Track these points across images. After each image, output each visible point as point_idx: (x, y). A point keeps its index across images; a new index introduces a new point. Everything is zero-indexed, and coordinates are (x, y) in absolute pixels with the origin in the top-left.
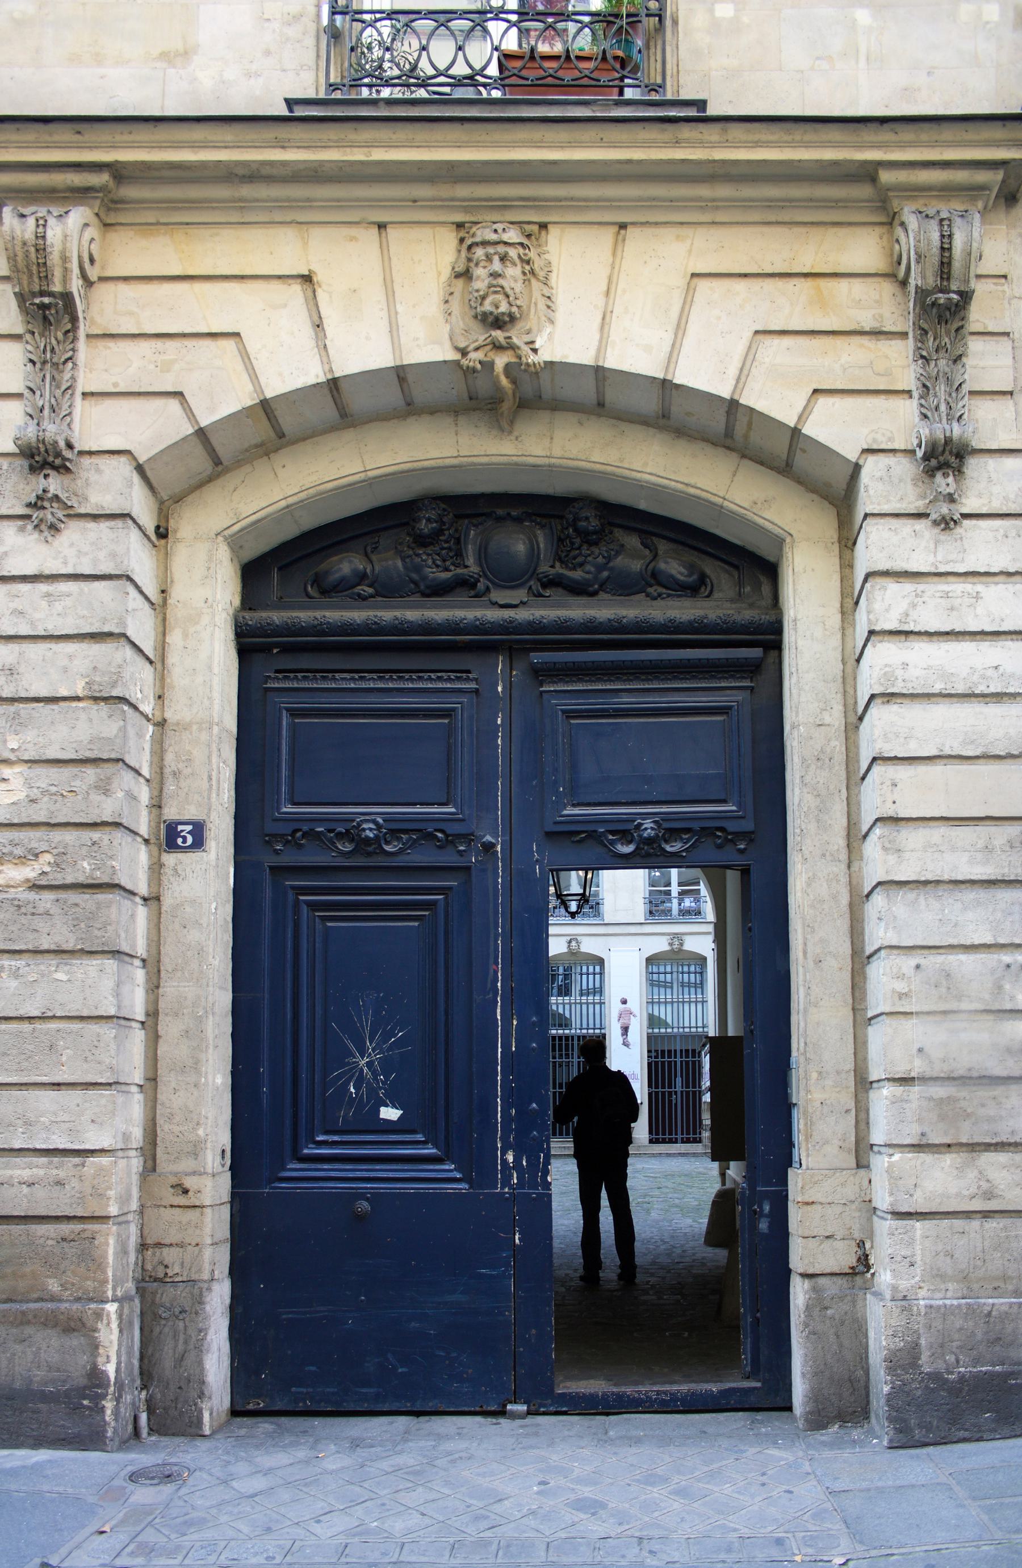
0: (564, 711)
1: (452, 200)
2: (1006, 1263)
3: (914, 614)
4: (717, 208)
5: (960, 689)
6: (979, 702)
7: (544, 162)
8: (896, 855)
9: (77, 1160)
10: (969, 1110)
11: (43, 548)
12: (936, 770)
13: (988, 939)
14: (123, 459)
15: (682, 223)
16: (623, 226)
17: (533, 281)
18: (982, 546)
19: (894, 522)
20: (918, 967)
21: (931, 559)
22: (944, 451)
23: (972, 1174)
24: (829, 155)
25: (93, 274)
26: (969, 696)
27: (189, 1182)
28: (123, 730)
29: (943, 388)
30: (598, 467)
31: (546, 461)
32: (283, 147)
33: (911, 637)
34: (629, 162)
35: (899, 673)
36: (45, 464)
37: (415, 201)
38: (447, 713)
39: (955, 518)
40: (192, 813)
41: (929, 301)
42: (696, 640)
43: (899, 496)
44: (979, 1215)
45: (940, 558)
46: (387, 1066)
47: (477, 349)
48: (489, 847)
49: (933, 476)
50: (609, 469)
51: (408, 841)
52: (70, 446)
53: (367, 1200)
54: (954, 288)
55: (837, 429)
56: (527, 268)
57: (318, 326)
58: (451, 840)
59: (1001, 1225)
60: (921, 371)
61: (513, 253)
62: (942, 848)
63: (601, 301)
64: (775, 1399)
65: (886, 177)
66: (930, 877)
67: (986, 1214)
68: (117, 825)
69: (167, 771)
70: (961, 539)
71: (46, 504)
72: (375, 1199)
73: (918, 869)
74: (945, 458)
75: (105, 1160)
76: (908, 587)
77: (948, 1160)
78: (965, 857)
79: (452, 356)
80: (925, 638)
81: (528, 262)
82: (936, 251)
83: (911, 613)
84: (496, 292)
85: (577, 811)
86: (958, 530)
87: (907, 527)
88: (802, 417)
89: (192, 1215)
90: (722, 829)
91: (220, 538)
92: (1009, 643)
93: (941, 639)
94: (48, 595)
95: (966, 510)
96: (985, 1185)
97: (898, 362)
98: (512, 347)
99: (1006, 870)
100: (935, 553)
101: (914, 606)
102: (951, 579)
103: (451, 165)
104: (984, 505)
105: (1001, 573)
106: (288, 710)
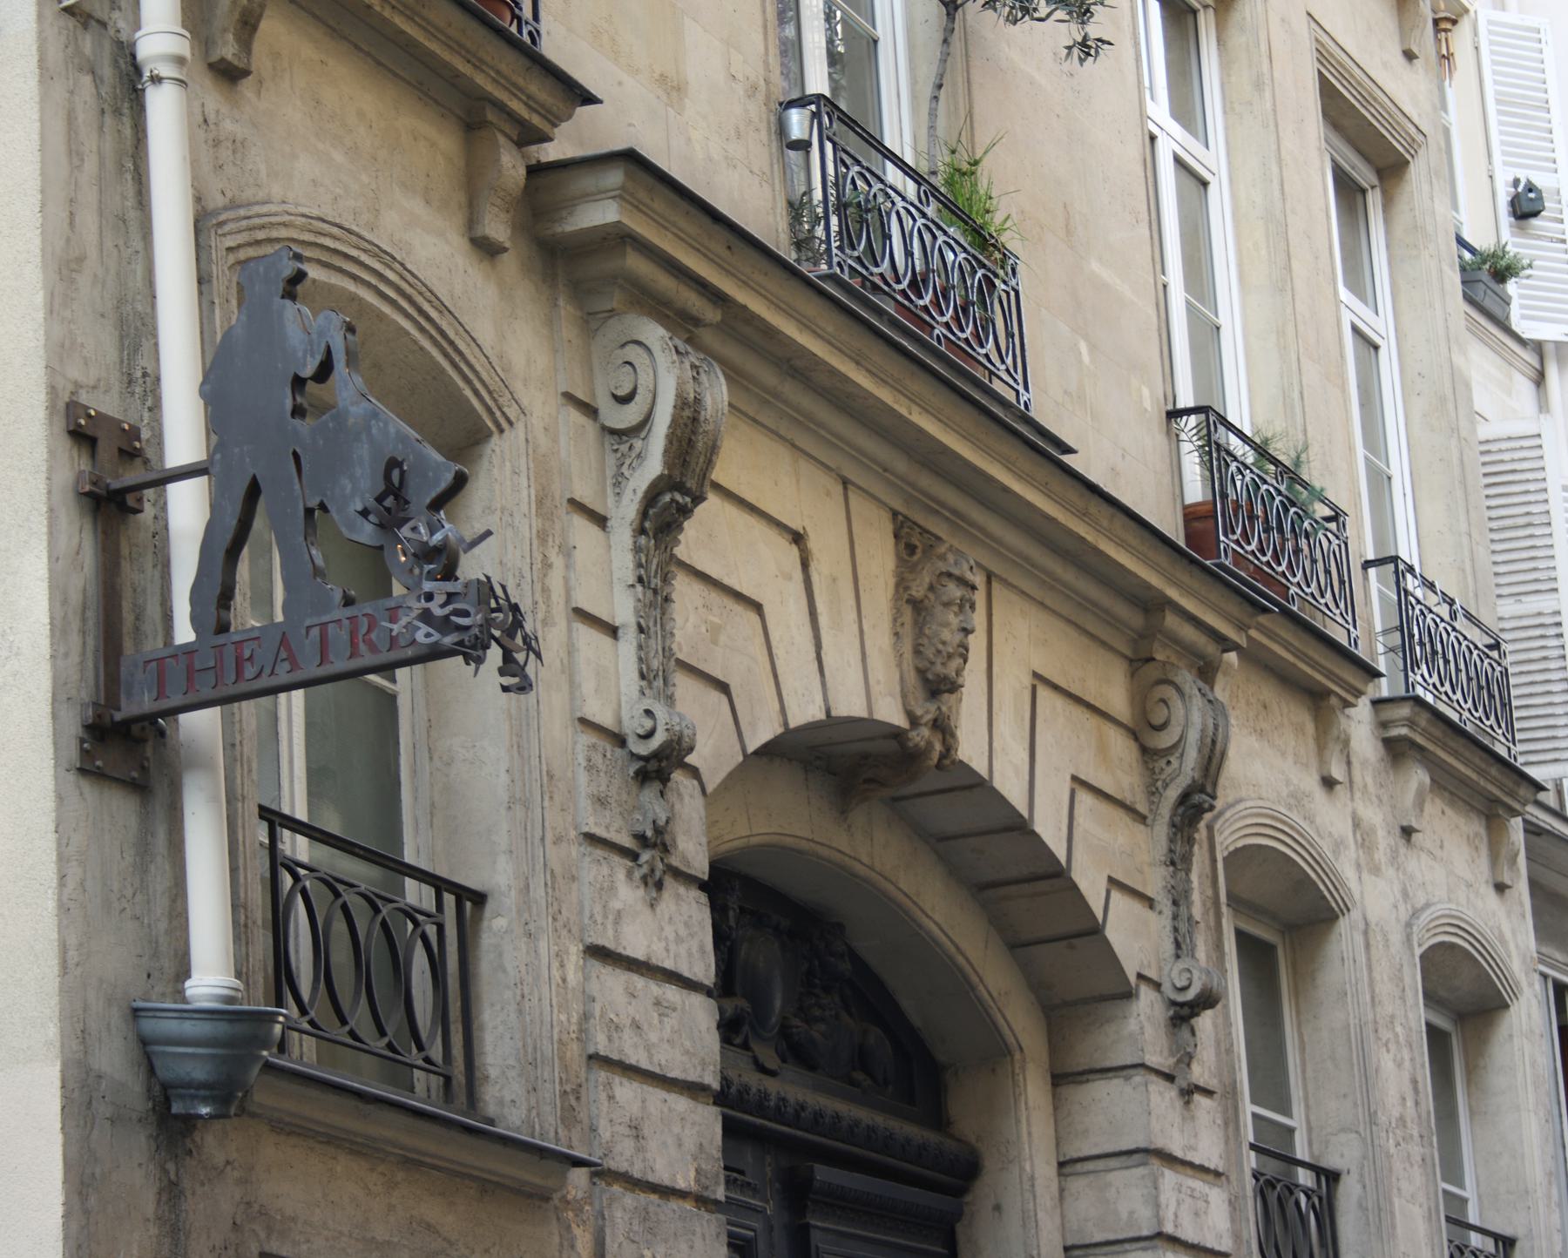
4: (1052, 588)
30: (901, 897)
32: (858, 363)
37: (885, 470)
65: (1171, 621)
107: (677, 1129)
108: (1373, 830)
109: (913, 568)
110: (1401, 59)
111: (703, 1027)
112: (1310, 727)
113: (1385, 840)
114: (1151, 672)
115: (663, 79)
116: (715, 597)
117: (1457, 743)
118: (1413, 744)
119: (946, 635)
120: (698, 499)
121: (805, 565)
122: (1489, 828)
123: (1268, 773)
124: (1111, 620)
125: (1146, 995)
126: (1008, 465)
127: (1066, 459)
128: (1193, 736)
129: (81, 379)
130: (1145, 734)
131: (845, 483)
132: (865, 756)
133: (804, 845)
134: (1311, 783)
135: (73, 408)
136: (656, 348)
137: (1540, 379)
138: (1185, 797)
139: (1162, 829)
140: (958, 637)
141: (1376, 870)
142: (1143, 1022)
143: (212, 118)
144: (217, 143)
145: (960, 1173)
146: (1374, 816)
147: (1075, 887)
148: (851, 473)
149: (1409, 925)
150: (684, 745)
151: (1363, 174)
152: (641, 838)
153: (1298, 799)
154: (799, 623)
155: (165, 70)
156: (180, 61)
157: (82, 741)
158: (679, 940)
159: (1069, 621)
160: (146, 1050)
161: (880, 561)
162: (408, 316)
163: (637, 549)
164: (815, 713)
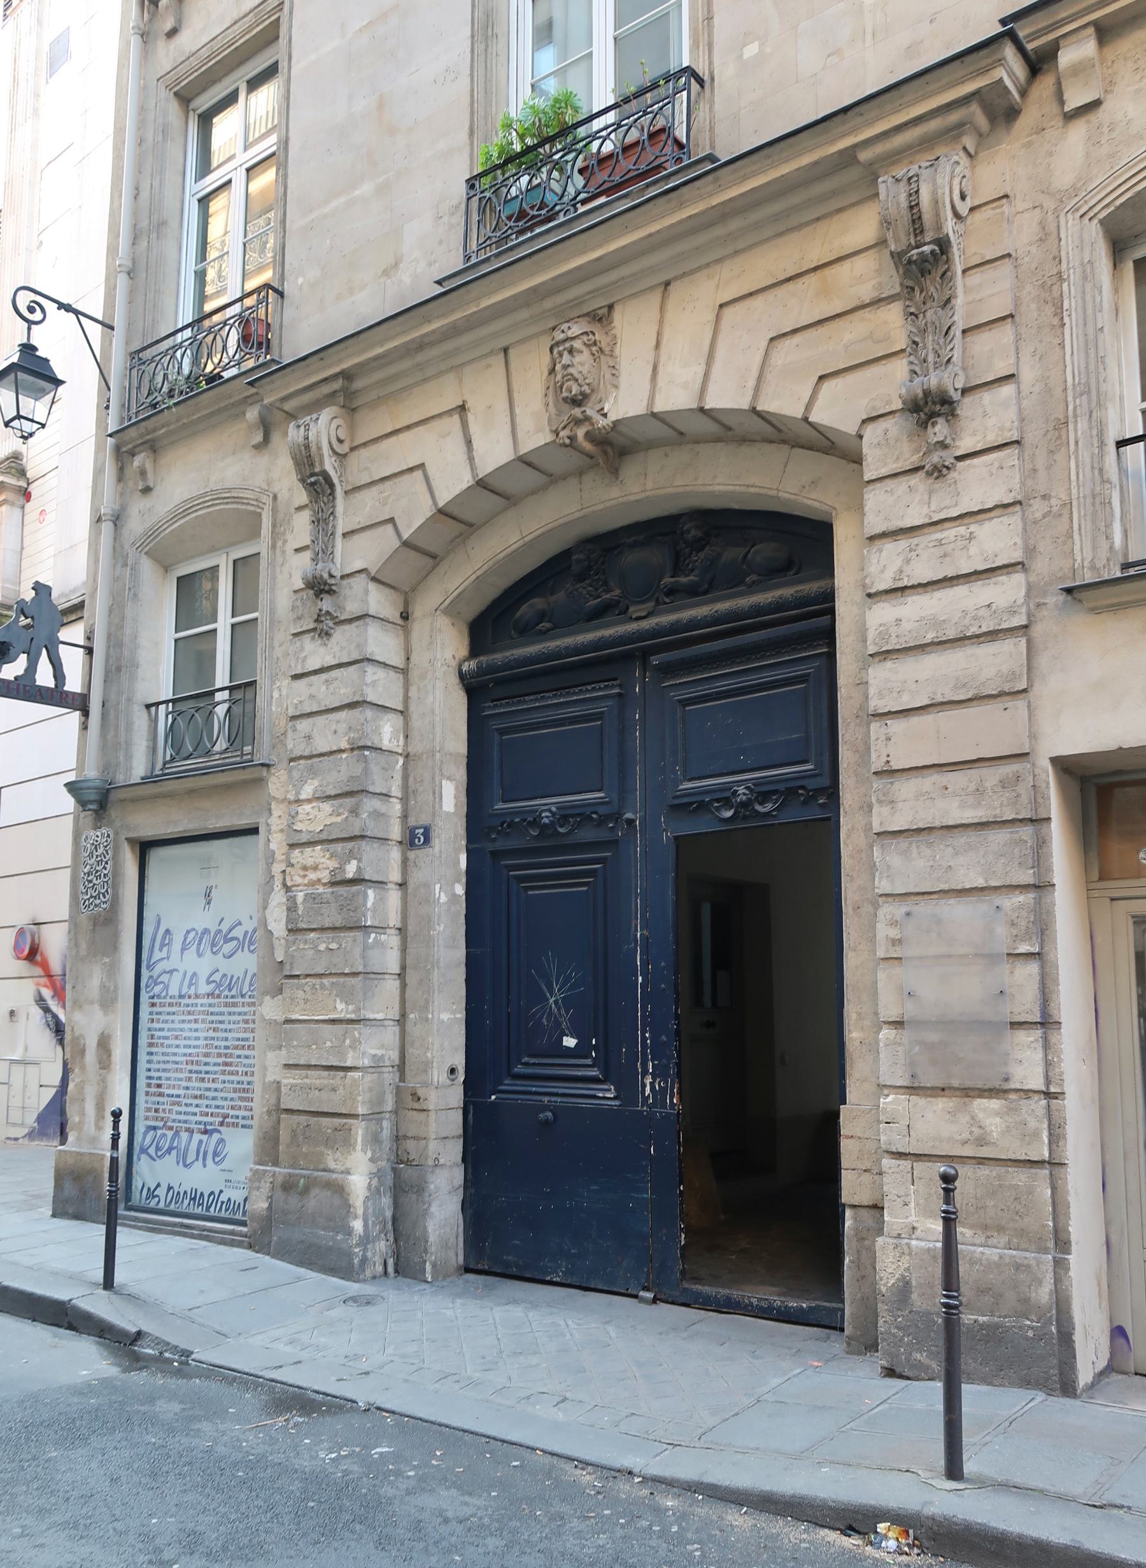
0: (679, 701)
1: (544, 312)
2: (999, 1212)
3: (907, 570)
5: (951, 634)
6: (973, 644)
7: (553, 279)
8: (890, 806)
9: (342, 1074)
10: (961, 1055)
11: (322, 650)
12: (928, 719)
13: (980, 882)
14: (363, 576)
15: (818, 219)
16: (667, 284)
17: (602, 357)
18: (979, 485)
19: (890, 484)
20: (908, 914)
21: (925, 510)
22: (926, 403)
23: (964, 1119)
24: (806, 160)
25: (963, 208)
26: (961, 640)
27: (421, 1093)
28: (366, 770)
29: (930, 338)
31: (643, 495)
33: (907, 592)
34: (650, 235)
35: (893, 631)
36: (322, 591)
38: (599, 716)
39: (947, 464)
40: (424, 820)
41: (904, 260)
42: (822, 609)
43: (895, 457)
44: (973, 1161)
45: (933, 508)
46: (567, 1002)
47: (564, 428)
48: (631, 822)
49: (926, 427)
50: (688, 488)
51: (574, 823)
52: (331, 576)
53: (551, 1111)
54: (928, 239)
55: (836, 411)
56: (594, 349)
57: (469, 442)
58: (602, 821)
59: (994, 1174)
60: (910, 328)
61: (577, 344)
62: (932, 795)
63: (652, 353)
65: (864, 156)
66: (921, 825)
67: (981, 1161)
68: (363, 837)
69: (410, 790)
70: (955, 482)
71: (323, 619)
73: (910, 818)
74: (930, 408)
75: (357, 1075)
76: (903, 544)
77: (941, 1104)
78: (955, 803)
80: (920, 590)
81: (595, 343)
82: (905, 212)
83: (905, 569)
84: (568, 380)
85: (690, 785)
86: (953, 475)
87: (902, 484)
88: (809, 407)
89: (423, 1115)
90: (802, 787)
91: (439, 612)
92: (1003, 578)
93: (935, 587)
95: (959, 453)
96: (977, 1131)
97: (892, 323)
98: (587, 419)
99: (998, 811)
100: (929, 504)
101: (908, 561)
102: (947, 525)
103: (534, 290)
104: (978, 442)
105: (996, 507)
106: (496, 730)
107: (334, 727)
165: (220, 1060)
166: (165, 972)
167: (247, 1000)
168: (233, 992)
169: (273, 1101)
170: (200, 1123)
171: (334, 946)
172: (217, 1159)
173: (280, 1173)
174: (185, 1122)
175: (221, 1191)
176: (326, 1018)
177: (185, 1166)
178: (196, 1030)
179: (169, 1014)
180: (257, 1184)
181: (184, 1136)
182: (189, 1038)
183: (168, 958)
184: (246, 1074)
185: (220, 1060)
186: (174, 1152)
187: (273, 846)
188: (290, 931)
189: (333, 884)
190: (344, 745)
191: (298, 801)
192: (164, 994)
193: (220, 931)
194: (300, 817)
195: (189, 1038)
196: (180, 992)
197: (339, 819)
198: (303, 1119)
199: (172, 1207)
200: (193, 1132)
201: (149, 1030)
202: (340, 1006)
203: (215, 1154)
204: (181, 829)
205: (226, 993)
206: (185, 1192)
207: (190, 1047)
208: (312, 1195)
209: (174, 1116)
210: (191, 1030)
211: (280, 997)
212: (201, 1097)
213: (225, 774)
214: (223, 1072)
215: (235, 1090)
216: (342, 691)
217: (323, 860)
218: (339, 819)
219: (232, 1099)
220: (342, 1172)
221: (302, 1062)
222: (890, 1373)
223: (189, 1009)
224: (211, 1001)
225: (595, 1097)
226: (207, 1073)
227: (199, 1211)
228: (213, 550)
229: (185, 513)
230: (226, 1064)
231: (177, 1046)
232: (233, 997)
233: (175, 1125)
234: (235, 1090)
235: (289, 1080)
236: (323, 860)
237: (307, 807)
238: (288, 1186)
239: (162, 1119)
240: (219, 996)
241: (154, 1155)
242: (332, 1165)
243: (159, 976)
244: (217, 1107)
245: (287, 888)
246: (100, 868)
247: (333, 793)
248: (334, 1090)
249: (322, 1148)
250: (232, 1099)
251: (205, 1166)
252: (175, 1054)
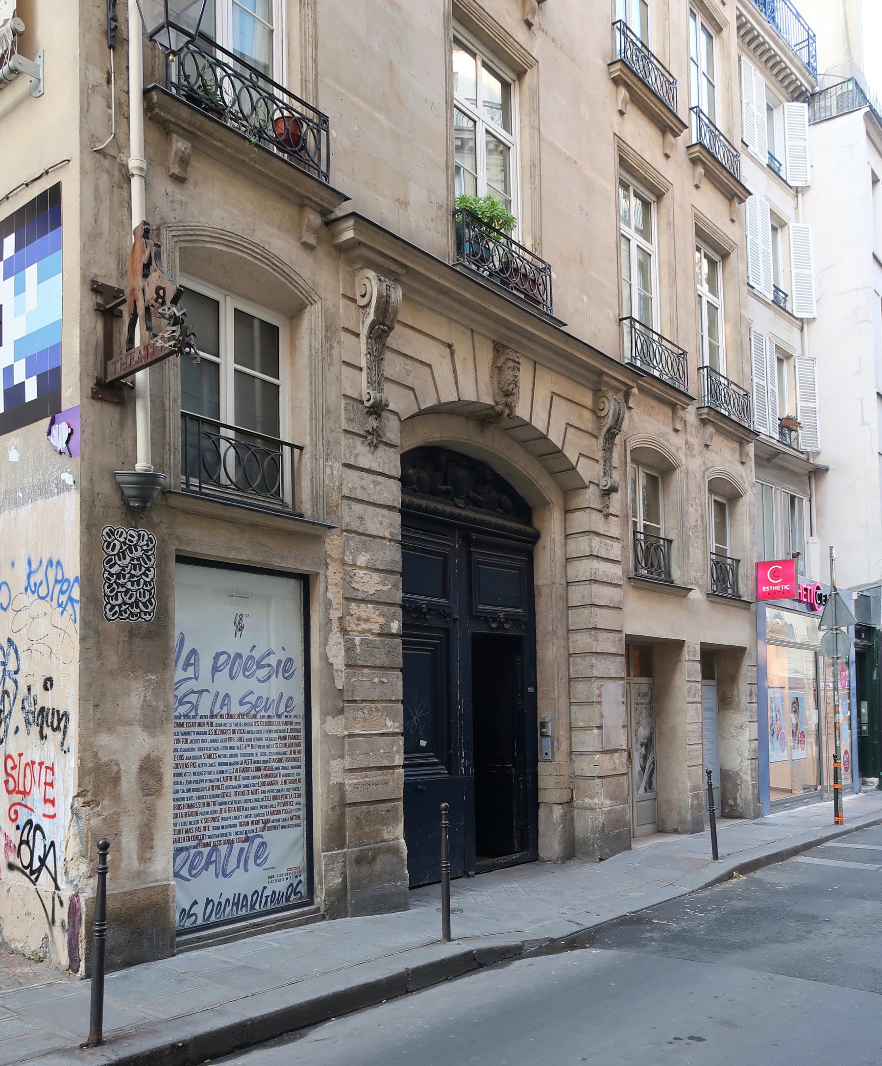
7: (517, 325)
11: (370, 455)
64: (535, 858)
65: (605, 378)
72: (425, 783)
79: (493, 404)
90: (520, 620)
94: (374, 481)
107: (380, 519)
108: (693, 445)
109: (498, 358)
110: (730, 222)
111: (394, 490)
112: (670, 414)
113: (697, 448)
114: (601, 393)
115: (398, 200)
116: (409, 362)
117: (727, 421)
118: (710, 421)
119: (508, 377)
120: (391, 329)
121: (452, 354)
122: (740, 446)
123: (645, 424)
124: (587, 379)
125: (592, 488)
126: (534, 327)
127: (562, 328)
128: (611, 412)
129: (98, 273)
130: (596, 412)
131: (472, 331)
132: (487, 415)
133: (465, 441)
134: (669, 430)
135: (94, 282)
136: (372, 279)
137: (802, 329)
138: (609, 430)
139: (601, 440)
140: (513, 378)
141: (693, 456)
142: (590, 497)
143: (170, 193)
144: (172, 202)
145: (536, 537)
146: (694, 441)
147: (565, 455)
148: (474, 327)
149: (704, 472)
150: (383, 402)
151: (716, 257)
152: (368, 432)
153: (663, 435)
154: (447, 370)
155: (135, 172)
156: (141, 169)
157: (92, 389)
158: (384, 463)
159: (569, 378)
160: (119, 487)
161: (486, 355)
162: (267, 265)
163: (367, 343)
164: (453, 398)
165: (259, 773)
166: (193, 692)
167: (283, 719)
168: (270, 713)
169: (337, 799)
170: (241, 833)
171: (385, 680)
172: (259, 861)
173: (352, 852)
174: (225, 835)
175: (265, 888)
176: (381, 732)
177: (225, 875)
178: (232, 748)
179: (198, 733)
180: (331, 866)
181: (223, 849)
182: (225, 756)
183: (196, 678)
184: (286, 782)
185: (259, 773)
186: (212, 867)
187: (329, 595)
188: (347, 666)
189: (379, 635)
190: (388, 535)
191: (354, 565)
192: (193, 713)
193: (252, 657)
194: (355, 578)
195: (225, 756)
196: (212, 712)
197: (385, 588)
198: (365, 808)
199: (213, 919)
200: (233, 842)
201: (176, 750)
202: (389, 723)
203: (257, 857)
204: (244, 558)
205: (263, 713)
206: (228, 900)
207: (226, 764)
208: (378, 860)
209: (211, 832)
210: (226, 748)
211: (340, 717)
212: (239, 809)
213: (279, 519)
214: (263, 784)
215: (274, 798)
216: (386, 495)
217: (373, 616)
218: (385, 588)
219: (271, 806)
220: (393, 840)
221: (363, 766)
222: (601, 860)
223: (222, 728)
224: (246, 720)
225: (440, 774)
226: (246, 786)
227: (243, 912)
228: (227, 288)
229: (229, 244)
230: (266, 776)
231: (211, 765)
232: (269, 717)
233: (212, 840)
234: (274, 798)
235: (349, 781)
236: (373, 616)
237: (362, 573)
238: (359, 860)
239: (196, 838)
240: (255, 716)
241: (188, 876)
242: (386, 836)
243: (185, 696)
244: (257, 815)
245: (344, 631)
246: (138, 573)
247: (380, 567)
248: (386, 783)
249: (380, 826)
250: (271, 806)
251: (246, 870)
252: (210, 773)
